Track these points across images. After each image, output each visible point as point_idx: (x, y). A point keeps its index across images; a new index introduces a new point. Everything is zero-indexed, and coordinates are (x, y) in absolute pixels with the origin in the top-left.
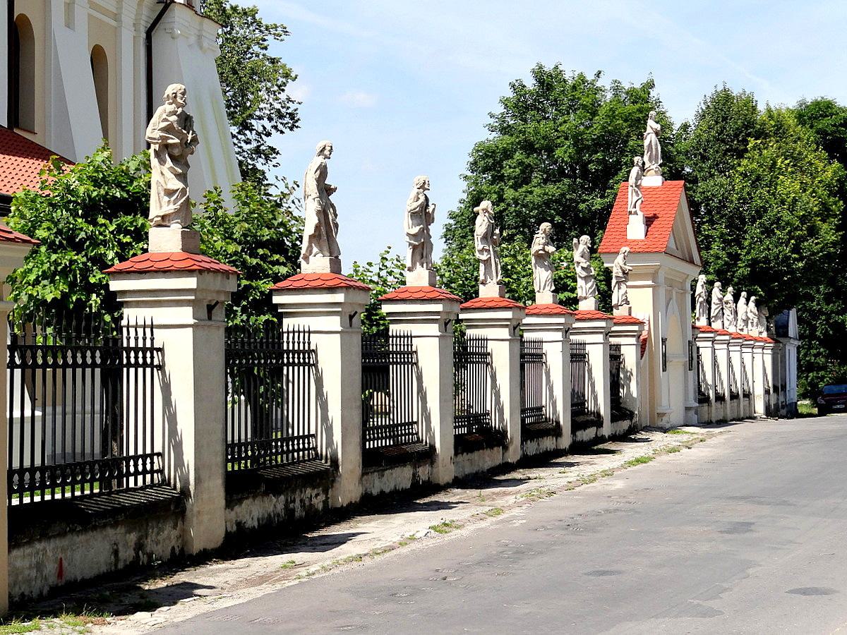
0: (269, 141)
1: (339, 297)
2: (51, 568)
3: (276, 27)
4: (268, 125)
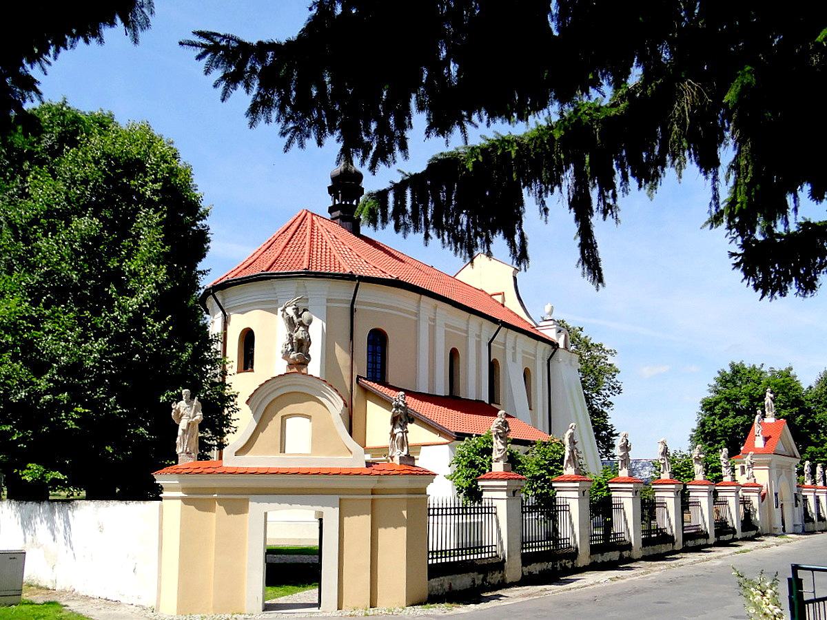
0: (609, 399)
1: (577, 484)
2: (446, 586)
3: (611, 351)
4: (608, 393)
